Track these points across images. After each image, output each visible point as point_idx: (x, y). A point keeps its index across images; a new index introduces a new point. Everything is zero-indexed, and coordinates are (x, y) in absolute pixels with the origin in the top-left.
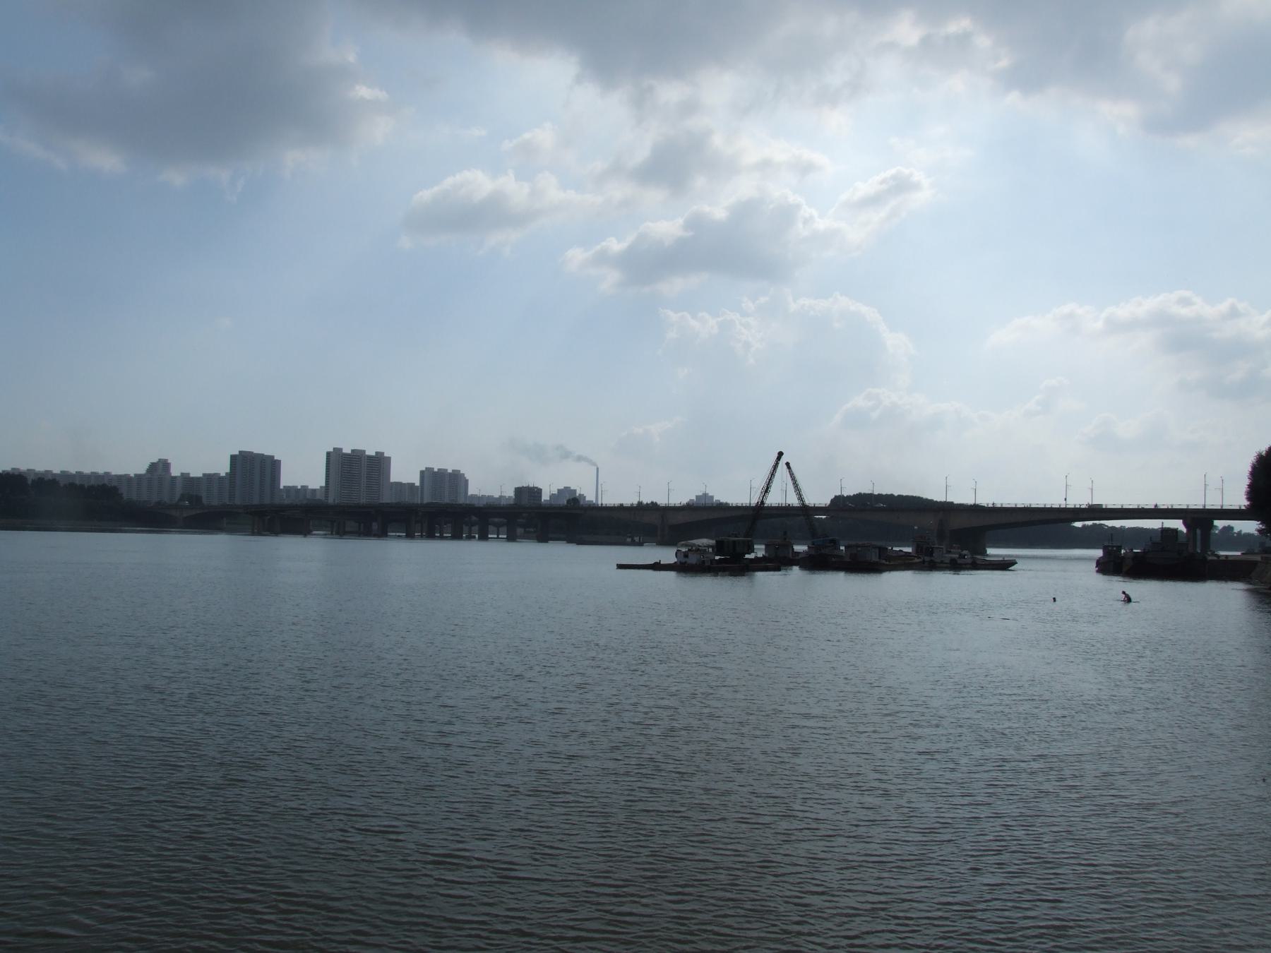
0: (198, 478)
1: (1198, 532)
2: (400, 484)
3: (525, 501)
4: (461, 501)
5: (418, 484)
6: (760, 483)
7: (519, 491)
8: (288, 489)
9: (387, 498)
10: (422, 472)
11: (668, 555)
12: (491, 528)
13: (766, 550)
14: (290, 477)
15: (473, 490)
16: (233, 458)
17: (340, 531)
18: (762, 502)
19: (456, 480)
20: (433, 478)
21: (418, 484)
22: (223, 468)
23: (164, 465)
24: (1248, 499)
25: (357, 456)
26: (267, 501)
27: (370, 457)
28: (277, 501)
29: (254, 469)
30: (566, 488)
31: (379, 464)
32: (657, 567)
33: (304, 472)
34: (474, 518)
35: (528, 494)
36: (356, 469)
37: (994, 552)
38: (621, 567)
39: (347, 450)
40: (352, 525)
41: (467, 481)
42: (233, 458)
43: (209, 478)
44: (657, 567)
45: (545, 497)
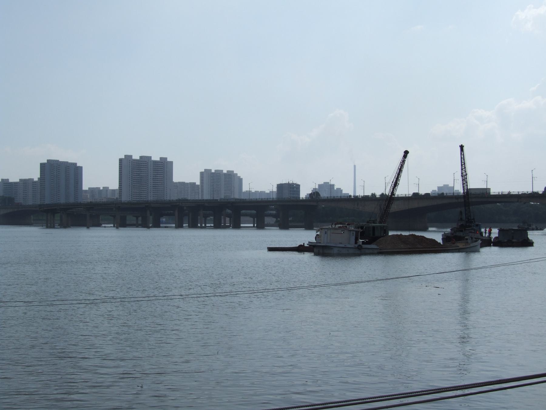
0: (15, 184)
1: (243, 211)
2: (183, 184)
3: (286, 195)
4: (237, 196)
5: (198, 183)
6: (391, 178)
7: (280, 187)
8: (92, 191)
9: (173, 196)
10: (202, 174)
11: (307, 237)
12: (242, 218)
13: (499, 233)
14: (88, 182)
15: (245, 188)
16: (42, 166)
17: (122, 224)
18: (393, 193)
19: (231, 179)
20: (211, 177)
21: (198, 183)
22: (35, 175)
23: (166, 158)
24: (315, 195)
25: (145, 161)
26: (72, 200)
27: (155, 162)
28: (242, 197)
29: (60, 173)
30: (326, 184)
31: (163, 167)
32: (301, 249)
33: (101, 176)
34: (229, 211)
35: (289, 190)
36: (142, 172)
37: (103, 225)
38: (271, 249)
39: (136, 157)
40: (130, 218)
41: (240, 180)
42: (42, 166)
43: (25, 183)
44: (301, 249)
45: (304, 194)
